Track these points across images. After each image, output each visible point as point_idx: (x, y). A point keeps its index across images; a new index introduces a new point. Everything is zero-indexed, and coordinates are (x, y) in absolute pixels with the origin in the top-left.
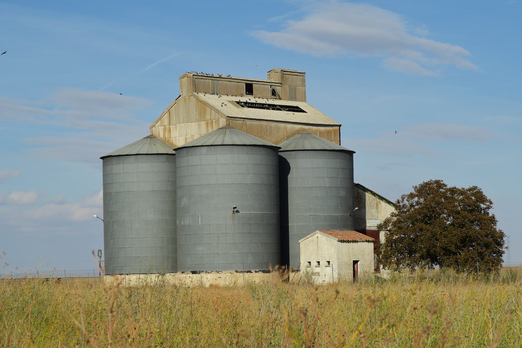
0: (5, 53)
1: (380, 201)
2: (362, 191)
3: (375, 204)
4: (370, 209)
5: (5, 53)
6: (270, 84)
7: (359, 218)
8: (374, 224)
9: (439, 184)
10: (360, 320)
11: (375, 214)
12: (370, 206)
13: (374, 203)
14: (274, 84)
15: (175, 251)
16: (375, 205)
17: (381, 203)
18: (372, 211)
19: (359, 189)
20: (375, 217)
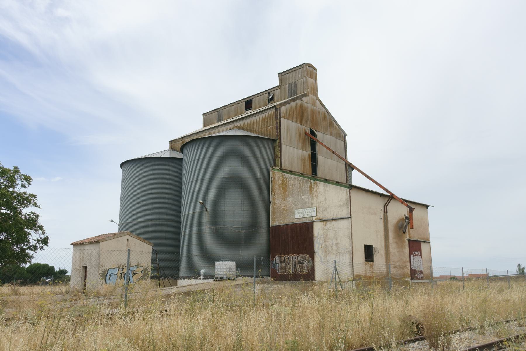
0: (112, 221)
1: (316, 182)
2: (290, 175)
3: (309, 187)
4: (300, 195)
5: (112, 221)
6: (267, 92)
7: (284, 209)
8: (305, 214)
9: (47, 265)
10: (101, 312)
11: (308, 201)
12: (300, 191)
13: (306, 187)
14: (271, 90)
15: (329, 220)
16: (309, 189)
17: (317, 185)
18: (303, 197)
19: (285, 174)
20: (307, 205)
